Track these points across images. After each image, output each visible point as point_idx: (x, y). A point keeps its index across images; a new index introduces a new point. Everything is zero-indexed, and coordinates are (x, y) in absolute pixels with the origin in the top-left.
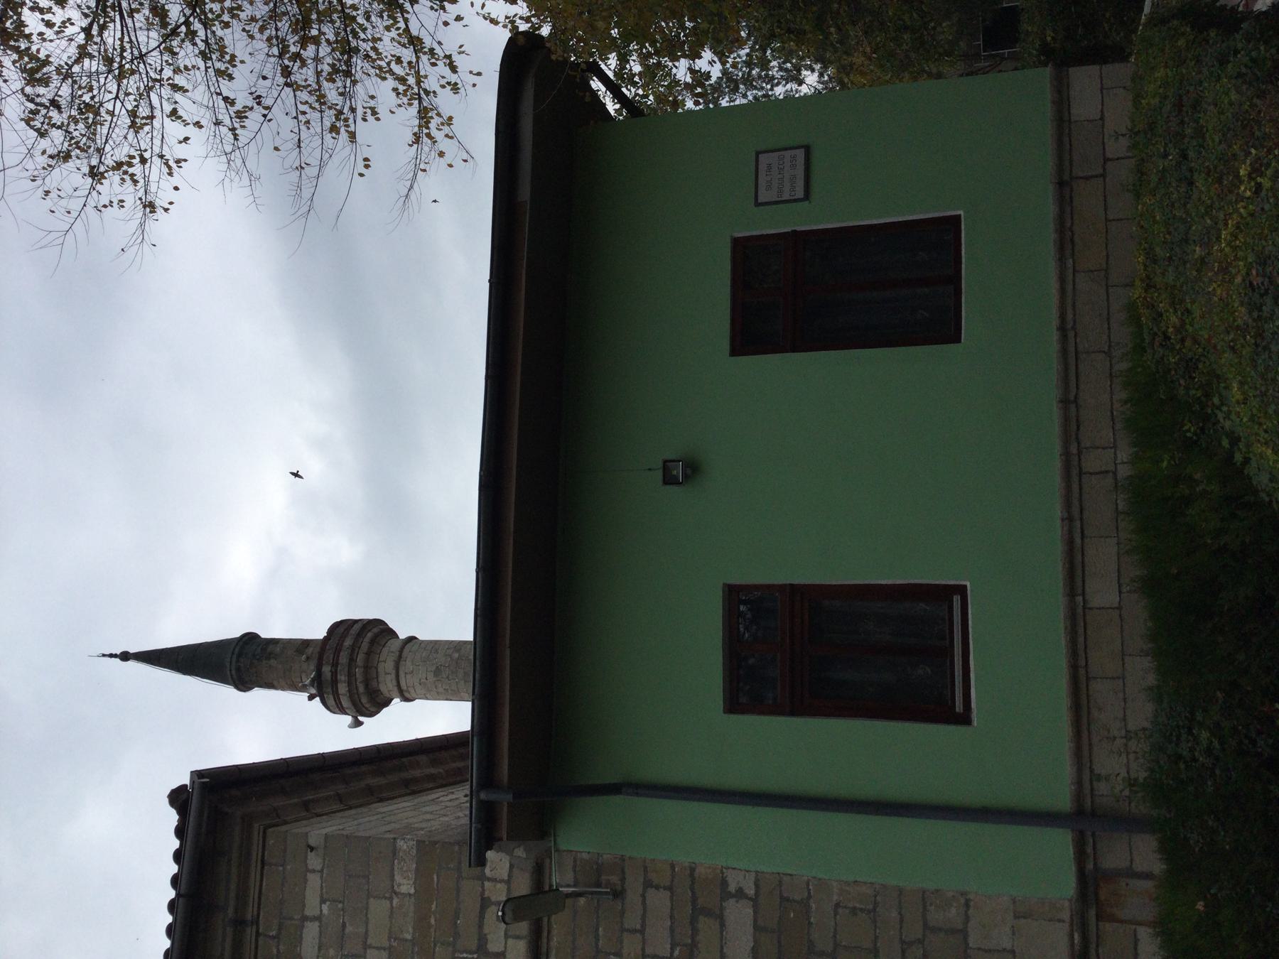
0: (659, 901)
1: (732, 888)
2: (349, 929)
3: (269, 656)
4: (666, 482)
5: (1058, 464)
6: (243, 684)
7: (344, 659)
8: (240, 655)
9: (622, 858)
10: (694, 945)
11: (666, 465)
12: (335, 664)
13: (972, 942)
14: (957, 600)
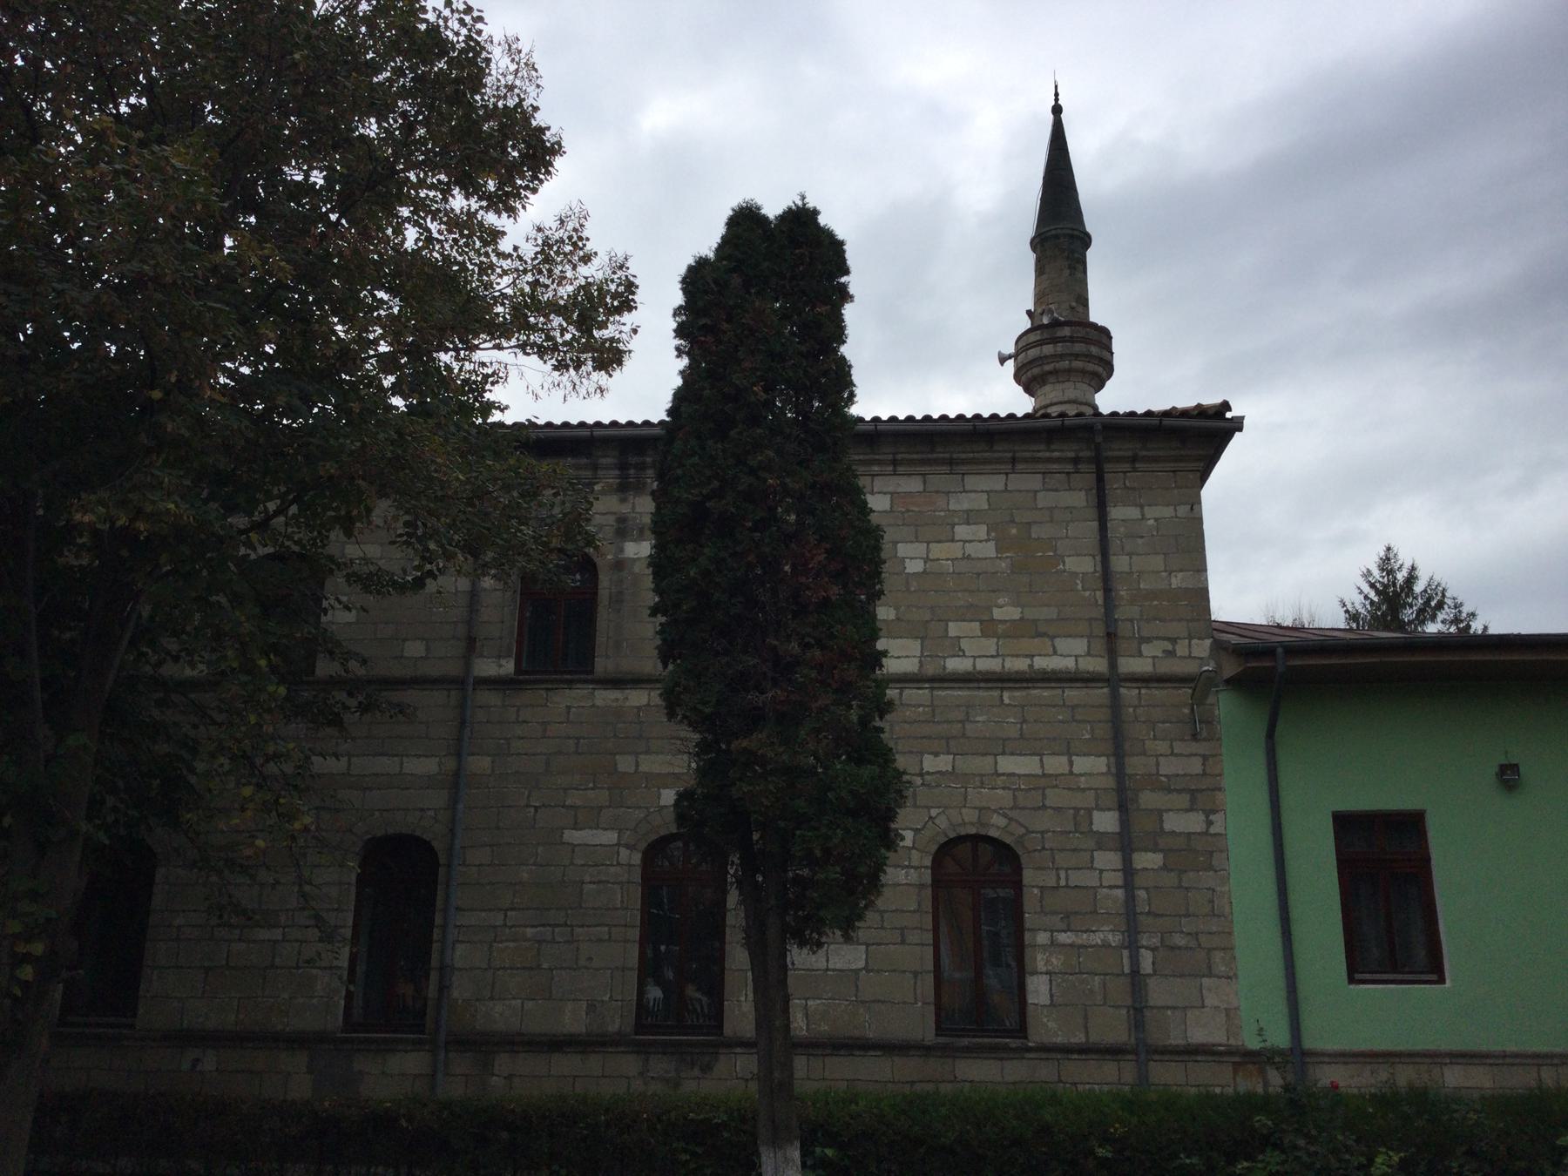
0: (1196, 766)
1: (1212, 817)
2: (1140, 541)
3: (1072, 268)
4: (1502, 766)
5: (1545, 1049)
6: (1038, 243)
7: (1079, 348)
8: (1072, 236)
9: (1219, 739)
10: (1170, 791)
11: (1514, 768)
12: (1072, 340)
13: (1205, 981)
14: (1434, 977)
